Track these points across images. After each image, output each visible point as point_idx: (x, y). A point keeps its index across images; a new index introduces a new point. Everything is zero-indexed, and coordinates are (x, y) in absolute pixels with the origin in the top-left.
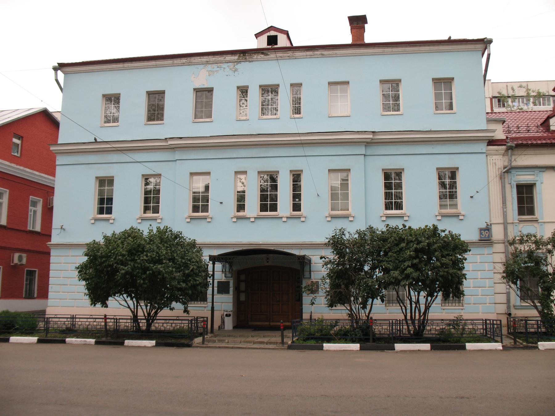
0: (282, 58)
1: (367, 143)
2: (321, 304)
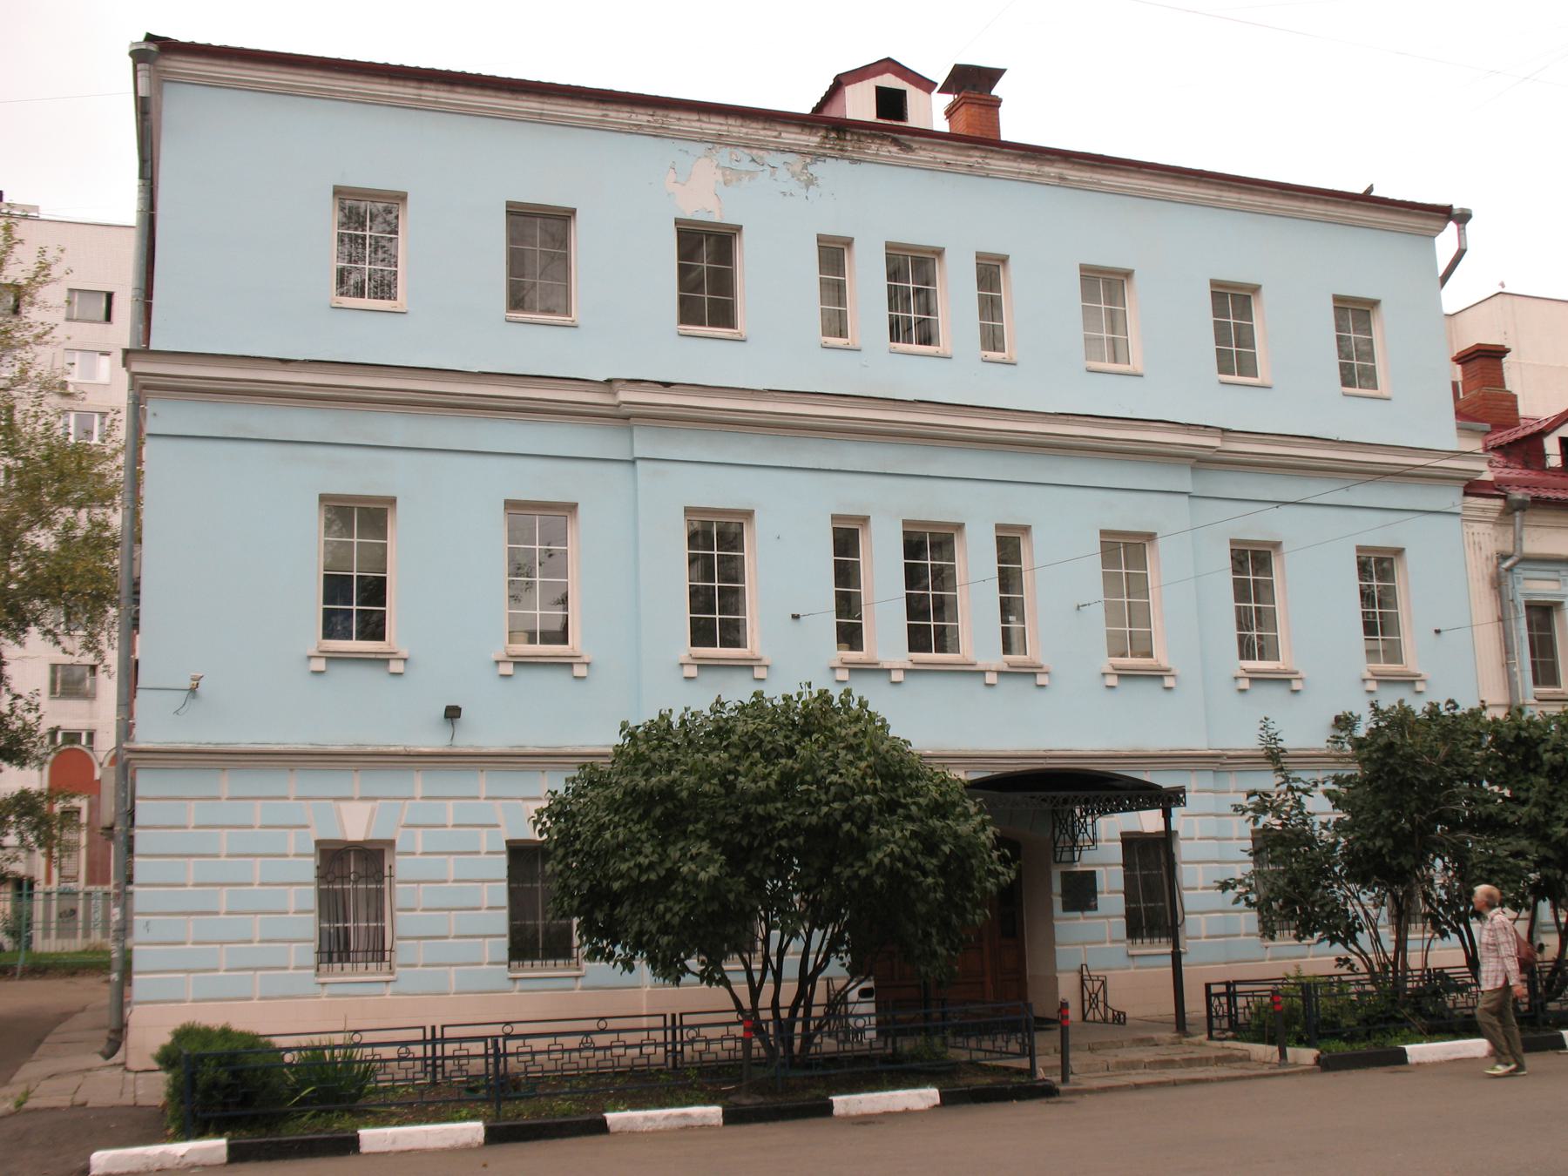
0: (950, 168)
1: (1201, 460)
2: (1105, 942)
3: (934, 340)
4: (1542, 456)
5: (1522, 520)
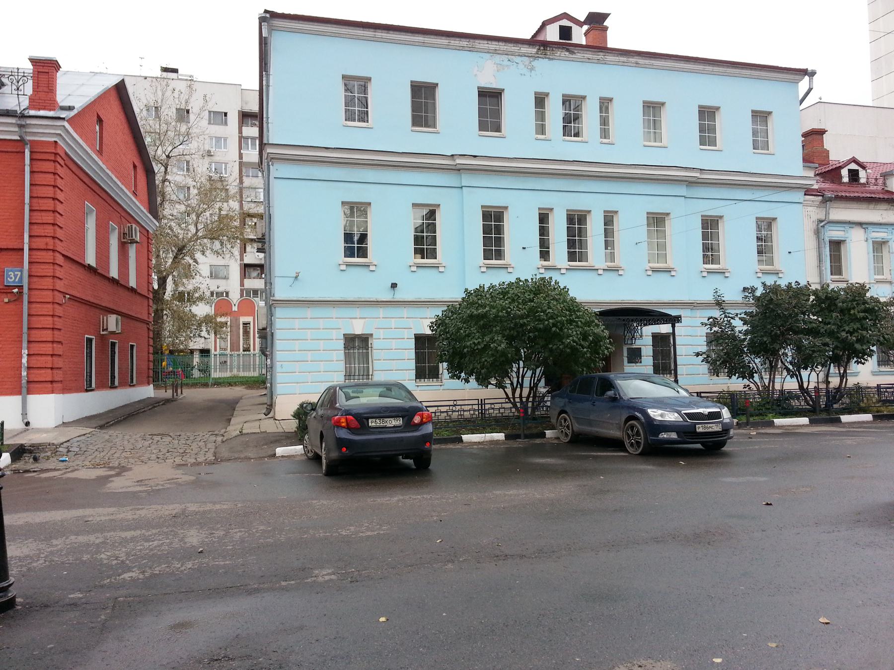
0: (590, 61)
3: (580, 134)
4: (841, 177)
5: (829, 206)
